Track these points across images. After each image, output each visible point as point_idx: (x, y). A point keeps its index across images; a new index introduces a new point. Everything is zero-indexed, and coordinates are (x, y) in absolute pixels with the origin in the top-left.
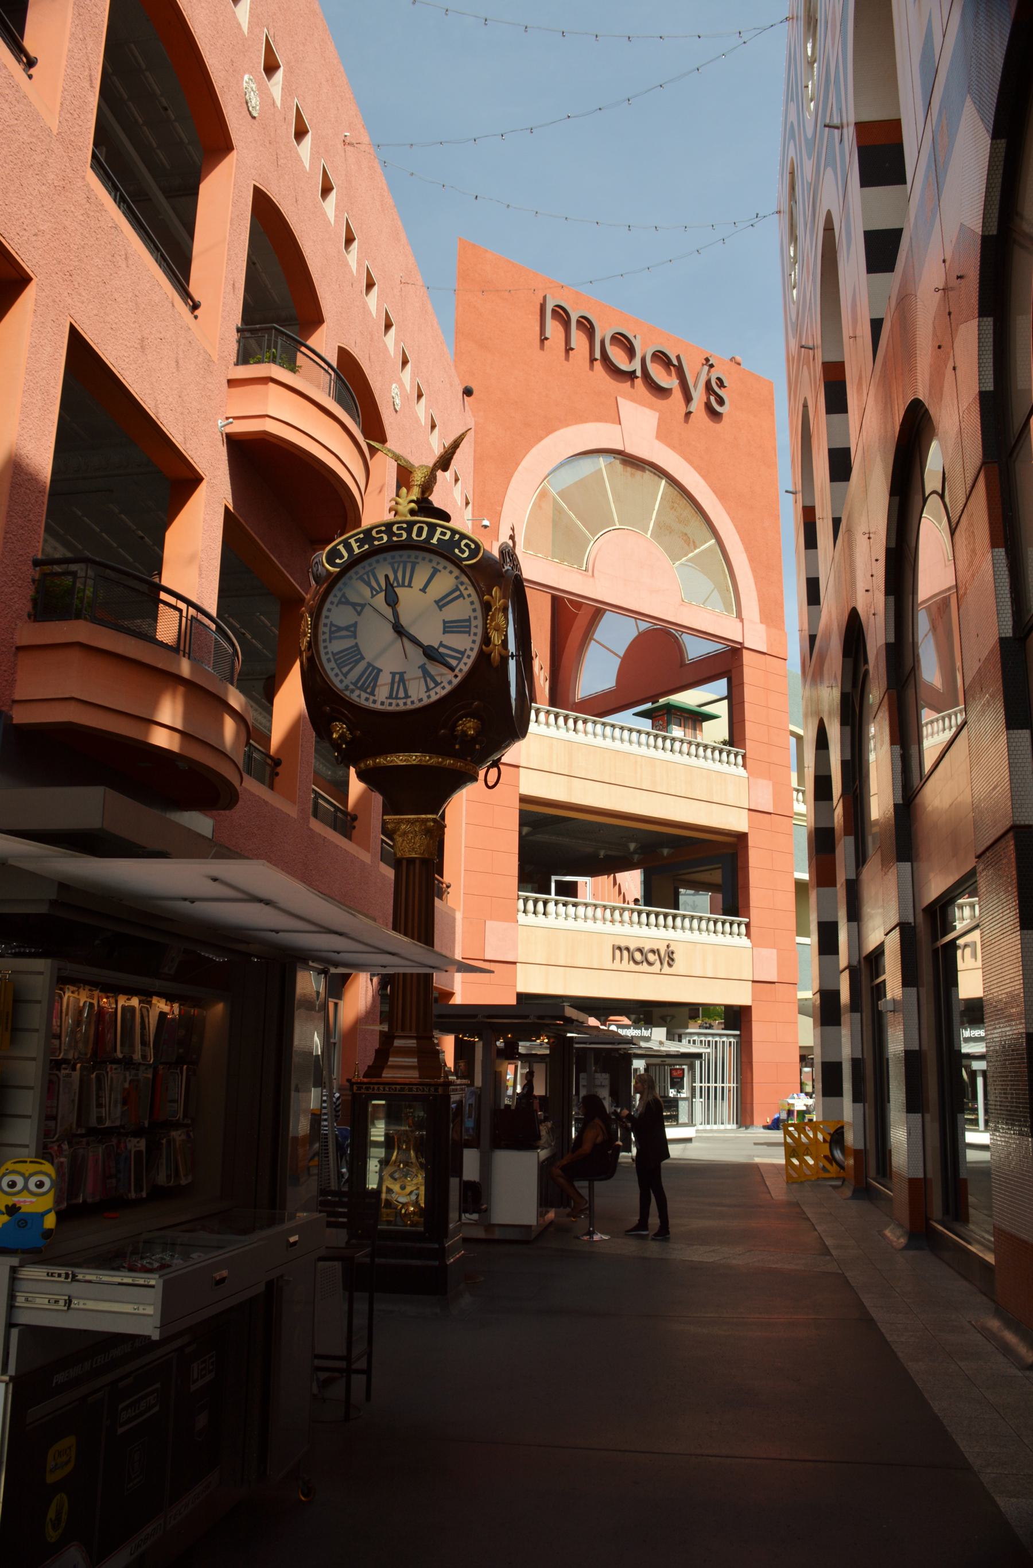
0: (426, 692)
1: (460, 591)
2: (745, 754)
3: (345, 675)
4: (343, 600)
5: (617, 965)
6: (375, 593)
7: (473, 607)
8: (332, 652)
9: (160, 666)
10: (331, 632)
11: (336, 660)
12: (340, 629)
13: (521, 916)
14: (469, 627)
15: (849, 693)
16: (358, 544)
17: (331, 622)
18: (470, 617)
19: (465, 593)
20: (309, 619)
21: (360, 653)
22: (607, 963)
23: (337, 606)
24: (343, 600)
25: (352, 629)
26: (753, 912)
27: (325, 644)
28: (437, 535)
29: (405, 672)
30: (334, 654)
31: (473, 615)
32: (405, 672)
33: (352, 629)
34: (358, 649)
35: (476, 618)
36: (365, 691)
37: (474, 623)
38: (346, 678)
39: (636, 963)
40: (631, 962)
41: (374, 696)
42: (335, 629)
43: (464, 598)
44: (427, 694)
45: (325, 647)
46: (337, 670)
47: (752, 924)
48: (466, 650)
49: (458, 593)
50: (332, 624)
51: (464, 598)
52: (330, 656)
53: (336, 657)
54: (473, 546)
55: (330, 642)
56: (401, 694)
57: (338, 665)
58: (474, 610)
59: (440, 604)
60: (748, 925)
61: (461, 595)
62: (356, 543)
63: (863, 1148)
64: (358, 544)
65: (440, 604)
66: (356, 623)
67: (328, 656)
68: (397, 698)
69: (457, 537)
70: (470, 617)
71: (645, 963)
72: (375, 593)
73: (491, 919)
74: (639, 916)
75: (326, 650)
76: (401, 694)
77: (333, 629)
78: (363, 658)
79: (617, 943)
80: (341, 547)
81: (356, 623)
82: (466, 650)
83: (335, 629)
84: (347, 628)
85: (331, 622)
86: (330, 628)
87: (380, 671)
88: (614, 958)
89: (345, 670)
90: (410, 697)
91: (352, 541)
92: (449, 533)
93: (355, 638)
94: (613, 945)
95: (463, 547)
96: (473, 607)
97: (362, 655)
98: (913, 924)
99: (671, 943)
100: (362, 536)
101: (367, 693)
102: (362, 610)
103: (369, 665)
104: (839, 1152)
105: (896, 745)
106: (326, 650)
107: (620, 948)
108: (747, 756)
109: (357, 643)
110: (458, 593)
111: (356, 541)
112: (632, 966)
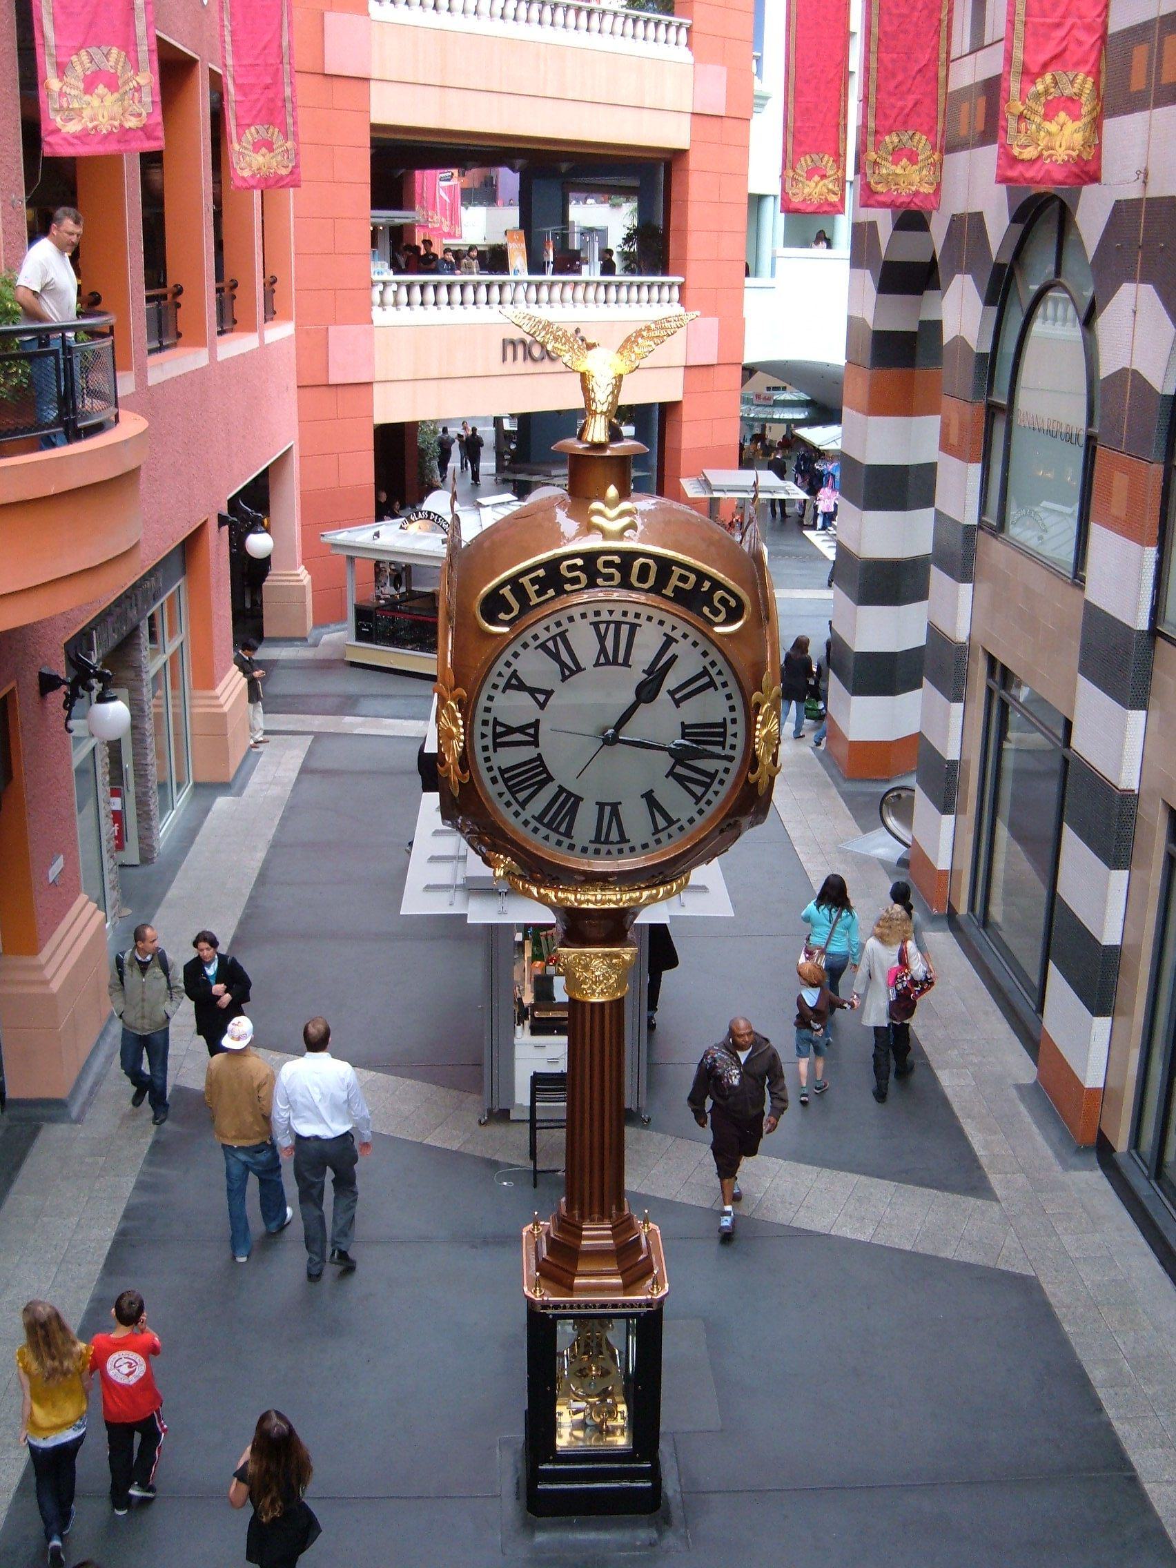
0: (653, 834)
1: (710, 676)
2: (691, 26)
3: (523, 805)
4: (514, 681)
5: (510, 367)
6: (567, 673)
7: (731, 703)
8: (499, 768)
9: (52, 491)
10: (496, 735)
11: (506, 781)
12: (510, 730)
13: (376, 312)
14: (724, 735)
15: (1005, 265)
16: (537, 587)
17: (495, 719)
18: (725, 719)
19: (718, 680)
20: (459, 715)
21: (545, 770)
22: (496, 366)
23: (504, 691)
24: (514, 681)
25: (532, 731)
26: (692, 267)
27: (486, 754)
28: (674, 581)
29: (620, 803)
30: (502, 772)
31: (729, 716)
32: (620, 803)
33: (532, 731)
34: (543, 764)
35: (734, 721)
36: (556, 830)
37: (731, 729)
38: (524, 809)
39: (534, 360)
40: (529, 359)
41: (571, 838)
42: (503, 729)
43: (716, 689)
44: (656, 837)
45: (487, 759)
46: (508, 796)
47: (690, 284)
48: (717, 771)
49: (706, 680)
50: (496, 723)
51: (716, 689)
52: (496, 773)
53: (506, 776)
54: (733, 603)
55: (495, 751)
56: (614, 836)
57: (509, 788)
58: (732, 709)
59: (677, 696)
60: (681, 287)
61: (711, 684)
62: (533, 585)
63: (949, 868)
64: (537, 587)
65: (677, 696)
66: (538, 721)
67: (492, 774)
68: (607, 842)
69: (707, 585)
70: (725, 719)
71: (547, 360)
72: (567, 673)
73: (335, 323)
74: (538, 290)
75: (488, 764)
76: (614, 836)
77: (499, 729)
78: (550, 779)
79: (509, 336)
80: (506, 591)
81: (538, 721)
82: (717, 771)
83: (503, 729)
84: (522, 729)
85: (495, 719)
86: (494, 729)
87: (579, 799)
88: (504, 359)
89: (522, 796)
90: (629, 841)
91: (525, 580)
92: (693, 578)
93: (537, 746)
94: (504, 340)
95: (723, 610)
96: (731, 703)
97: (548, 773)
98: (1136, 792)
99: (580, 326)
100: (541, 573)
101: (560, 833)
102: (546, 701)
103: (561, 789)
104: (893, 818)
105: (1152, 546)
106: (488, 764)
107: (513, 343)
108: (695, 28)
109: (539, 755)
110: (706, 680)
111: (533, 581)
112: (530, 366)
